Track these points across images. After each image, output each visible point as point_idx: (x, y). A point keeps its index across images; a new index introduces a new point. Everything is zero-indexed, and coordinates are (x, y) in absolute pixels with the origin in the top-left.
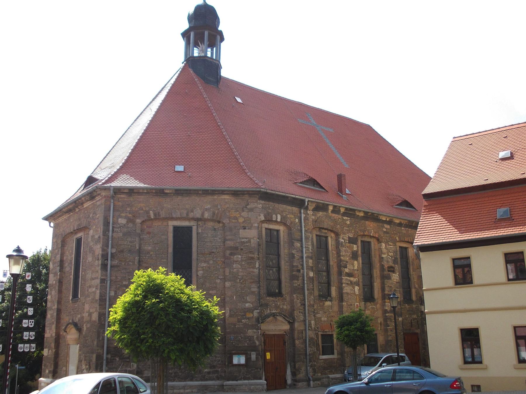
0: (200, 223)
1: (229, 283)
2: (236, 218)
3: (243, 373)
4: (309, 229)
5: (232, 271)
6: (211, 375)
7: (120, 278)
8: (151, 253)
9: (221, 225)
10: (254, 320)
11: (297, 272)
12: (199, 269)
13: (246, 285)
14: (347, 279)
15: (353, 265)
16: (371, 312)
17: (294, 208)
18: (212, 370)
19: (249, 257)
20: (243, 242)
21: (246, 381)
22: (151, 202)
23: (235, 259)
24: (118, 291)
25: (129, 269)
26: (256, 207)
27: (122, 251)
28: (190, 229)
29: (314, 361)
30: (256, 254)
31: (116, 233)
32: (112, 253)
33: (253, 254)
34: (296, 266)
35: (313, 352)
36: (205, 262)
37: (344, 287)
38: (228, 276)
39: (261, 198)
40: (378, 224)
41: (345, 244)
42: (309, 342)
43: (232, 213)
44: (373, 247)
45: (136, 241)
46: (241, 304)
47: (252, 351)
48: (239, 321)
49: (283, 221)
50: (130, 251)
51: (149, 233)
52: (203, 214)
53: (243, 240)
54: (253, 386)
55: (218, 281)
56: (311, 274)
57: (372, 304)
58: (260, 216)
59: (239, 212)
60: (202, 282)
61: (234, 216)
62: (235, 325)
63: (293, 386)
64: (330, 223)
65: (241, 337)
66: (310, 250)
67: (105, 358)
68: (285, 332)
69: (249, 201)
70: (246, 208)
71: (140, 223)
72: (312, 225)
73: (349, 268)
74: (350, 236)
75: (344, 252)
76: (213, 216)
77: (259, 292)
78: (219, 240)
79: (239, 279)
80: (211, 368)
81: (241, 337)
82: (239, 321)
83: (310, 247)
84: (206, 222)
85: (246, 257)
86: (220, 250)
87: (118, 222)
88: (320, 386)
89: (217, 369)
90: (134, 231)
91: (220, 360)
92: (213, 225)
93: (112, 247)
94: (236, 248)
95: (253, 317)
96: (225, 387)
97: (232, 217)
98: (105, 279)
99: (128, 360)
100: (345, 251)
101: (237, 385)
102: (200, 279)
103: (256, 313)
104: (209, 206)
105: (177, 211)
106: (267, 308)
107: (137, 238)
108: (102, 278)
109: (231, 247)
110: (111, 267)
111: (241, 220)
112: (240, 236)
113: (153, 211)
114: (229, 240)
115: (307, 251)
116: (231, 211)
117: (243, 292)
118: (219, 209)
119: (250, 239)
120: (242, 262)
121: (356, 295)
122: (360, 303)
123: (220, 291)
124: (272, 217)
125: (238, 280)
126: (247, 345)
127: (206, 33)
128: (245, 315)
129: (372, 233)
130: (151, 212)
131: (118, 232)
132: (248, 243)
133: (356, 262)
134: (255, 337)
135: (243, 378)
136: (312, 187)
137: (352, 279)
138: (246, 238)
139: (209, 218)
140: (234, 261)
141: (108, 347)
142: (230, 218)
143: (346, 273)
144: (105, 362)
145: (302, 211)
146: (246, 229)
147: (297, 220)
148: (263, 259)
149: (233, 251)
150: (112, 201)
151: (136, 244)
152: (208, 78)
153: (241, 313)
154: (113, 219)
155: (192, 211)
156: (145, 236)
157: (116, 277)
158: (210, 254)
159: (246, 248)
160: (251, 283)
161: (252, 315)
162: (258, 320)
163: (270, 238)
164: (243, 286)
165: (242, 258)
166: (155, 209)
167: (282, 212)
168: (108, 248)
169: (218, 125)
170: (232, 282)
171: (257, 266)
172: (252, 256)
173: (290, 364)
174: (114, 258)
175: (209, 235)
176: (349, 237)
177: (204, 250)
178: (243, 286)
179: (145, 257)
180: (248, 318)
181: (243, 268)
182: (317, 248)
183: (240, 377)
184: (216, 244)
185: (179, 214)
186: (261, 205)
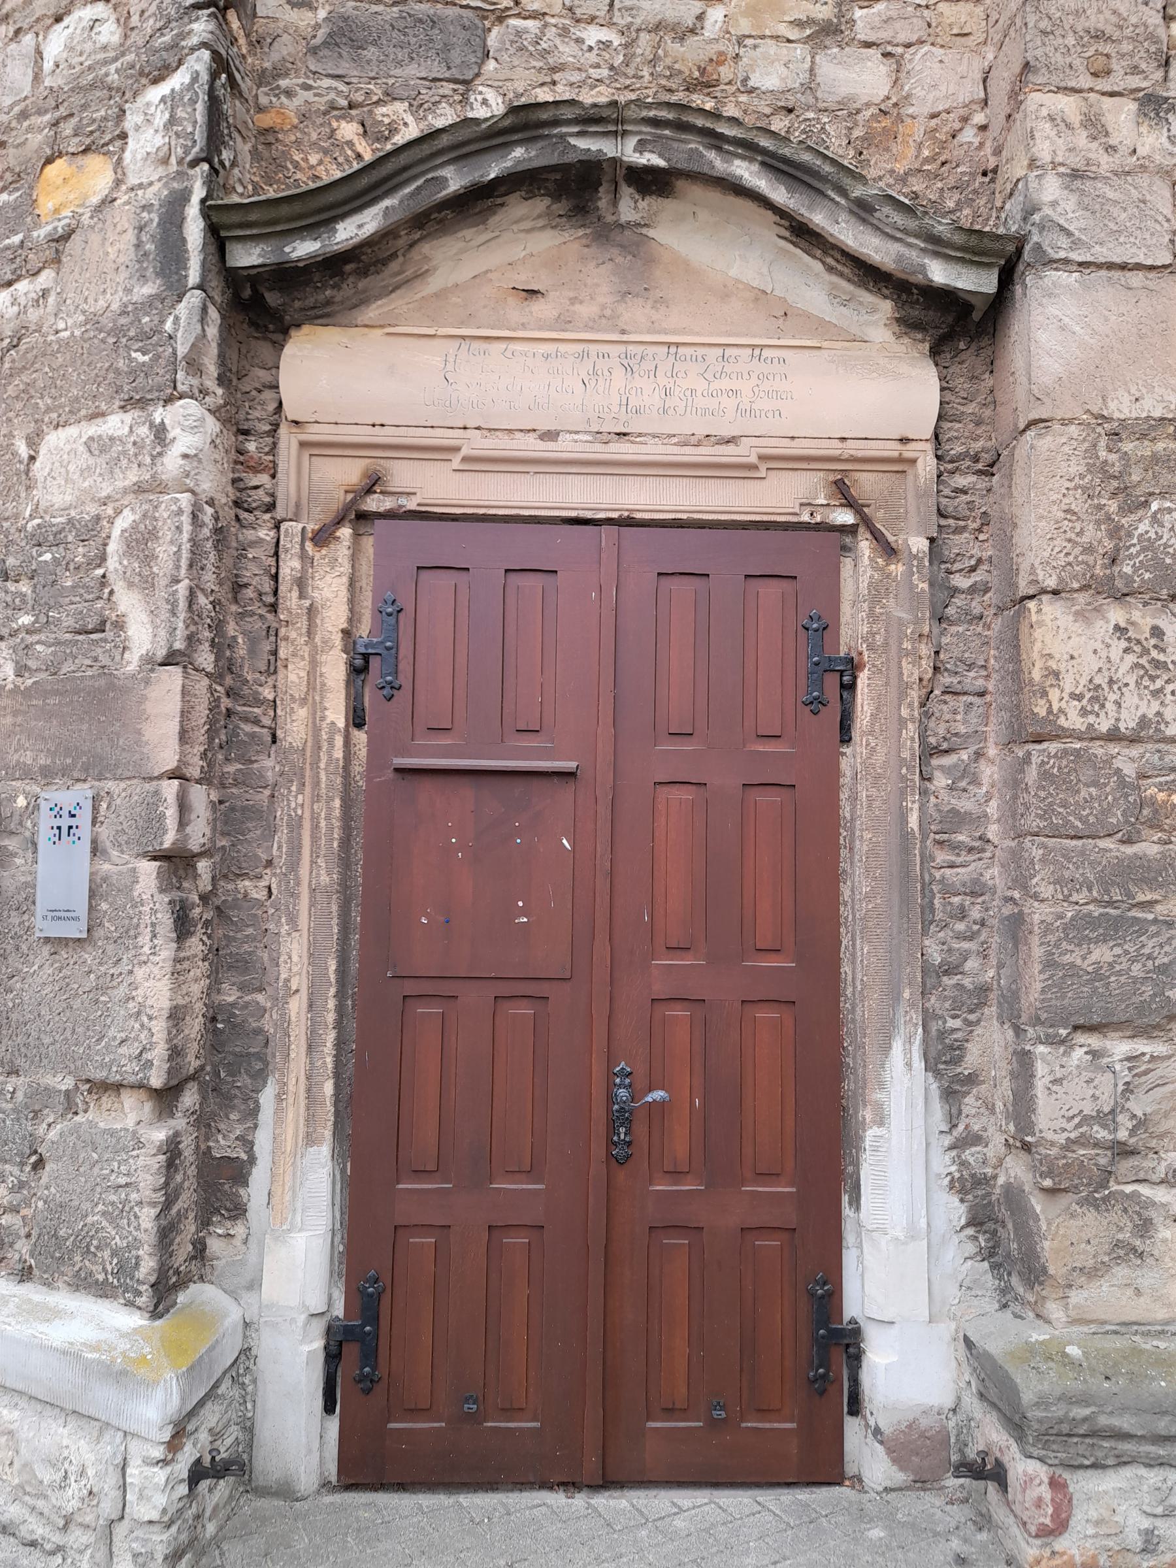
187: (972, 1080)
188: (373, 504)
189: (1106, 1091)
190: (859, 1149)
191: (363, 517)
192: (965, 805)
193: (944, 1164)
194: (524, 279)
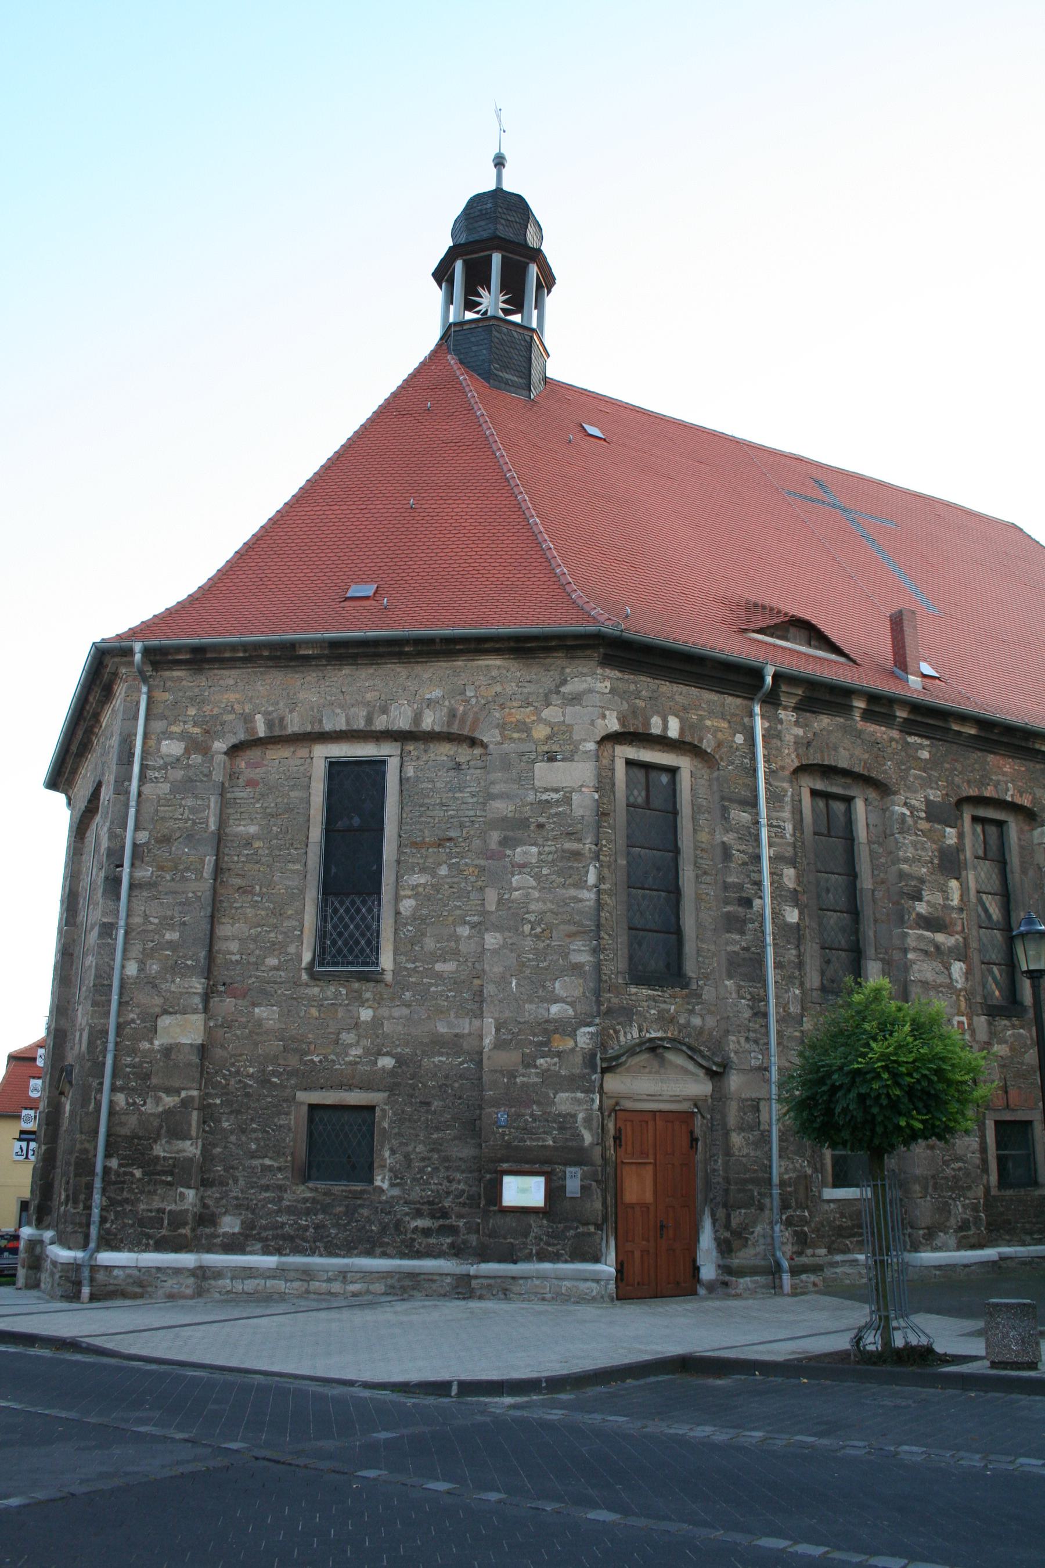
0: (411, 748)
1: (498, 935)
2: (524, 727)
3: (536, 1238)
4: (783, 768)
5: (506, 896)
6: (432, 1241)
7: (156, 921)
8: (257, 844)
9: (478, 751)
10: (578, 1059)
11: (739, 905)
12: (402, 893)
13: (553, 944)
14: (920, 938)
15: (944, 890)
16: (1012, 1049)
17: (729, 700)
18: (437, 1224)
19: (563, 851)
20: (547, 801)
21: (547, 1266)
22: (261, 688)
23: (518, 859)
24: (149, 962)
25: (183, 893)
26: (590, 691)
27: (165, 840)
28: (378, 765)
29: (801, 1206)
30: (588, 841)
31: (153, 784)
32: (135, 845)
33: (579, 840)
34: (734, 885)
35: (798, 1177)
36: (423, 870)
37: (913, 962)
38: (492, 912)
39: (607, 661)
40: (1031, 765)
41: (916, 823)
42: (781, 1140)
43: (513, 711)
44: (1016, 839)
45: (209, 809)
46: (533, 1006)
47: (571, 1165)
48: (528, 1063)
49: (688, 739)
50: (189, 837)
51: (251, 783)
52: (417, 718)
53: (545, 797)
54: (567, 1283)
55: (464, 931)
56: (792, 916)
57: (1017, 1023)
58: (604, 717)
59: (536, 708)
60: (413, 934)
61: (518, 721)
62: (512, 1075)
63: (721, 1287)
64: (858, 752)
65: (532, 1115)
66: (788, 836)
67: (99, 1168)
68: (696, 1106)
69: (568, 670)
70: (558, 692)
71: (225, 753)
72: (793, 756)
73: (928, 902)
74: (932, 798)
75: (911, 849)
76: (450, 724)
77: (598, 967)
78: (471, 800)
79: (530, 922)
80: (433, 1217)
81: (532, 1115)
82: (528, 1063)
83: (789, 827)
84: (432, 746)
85: (556, 852)
86: (472, 832)
87: (159, 750)
88: (817, 1292)
89: (453, 1221)
90: (206, 776)
91: (463, 1191)
92: (452, 753)
93: (137, 828)
94: (523, 823)
95: (573, 1050)
96: (474, 1282)
97: (512, 723)
98: (112, 924)
99: (169, 1179)
100: (914, 844)
101: (513, 1278)
102: (406, 924)
103: (584, 1037)
104: (437, 693)
105: (338, 711)
106: (631, 1021)
107: (213, 799)
108: (105, 920)
109: (504, 819)
110: (132, 886)
111: (540, 732)
112: (537, 783)
113: (266, 714)
114: (501, 796)
115: (777, 840)
116: (509, 704)
117: (541, 965)
118: (468, 701)
119: (571, 793)
120: (542, 867)
121: (957, 992)
122: (970, 1019)
123: (470, 964)
124: (647, 724)
125: (527, 928)
126: (551, 1143)
127: (497, 259)
128: (547, 1043)
129: (1010, 793)
130: (258, 717)
131: (158, 782)
132: (561, 805)
133: (954, 884)
134: (581, 1116)
135: (538, 1254)
136: (803, 649)
137: (940, 937)
138: (556, 790)
139: (437, 729)
140: (513, 866)
141: (109, 1135)
142: (502, 727)
143: (919, 915)
144: (98, 1184)
145: (757, 709)
146: (556, 760)
147: (739, 739)
148: (616, 861)
149: (510, 834)
150: (144, 689)
151: (208, 817)
152: (501, 374)
153: (534, 1035)
154: (144, 743)
155: (385, 711)
156: (240, 794)
157: (146, 916)
158: (439, 845)
159: (554, 823)
160: (569, 936)
161: (570, 1044)
162: (590, 1060)
163: (643, 793)
164: (541, 945)
165: (540, 853)
166: (270, 709)
167: (685, 709)
168: (125, 828)
169: (507, 479)
170: (507, 934)
171: (592, 878)
172: (575, 846)
173: (713, 1215)
174: (143, 862)
175: (438, 785)
176: (928, 802)
177: (421, 830)
178: (541, 945)
179: (236, 858)
180: (559, 1054)
181: (544, 888)
182: (815, 834)
183: (527, 1251)
184: (460, 813)
185: (343, 720)
186: (608, 684)
187: (717, 1220)
188: (617, 1108)
189: (742, 1218)
190: (613, 1366)
191: (616, 1111)
192: (716, 1167)
193: (713, 1236)
194: (642, 1064)
